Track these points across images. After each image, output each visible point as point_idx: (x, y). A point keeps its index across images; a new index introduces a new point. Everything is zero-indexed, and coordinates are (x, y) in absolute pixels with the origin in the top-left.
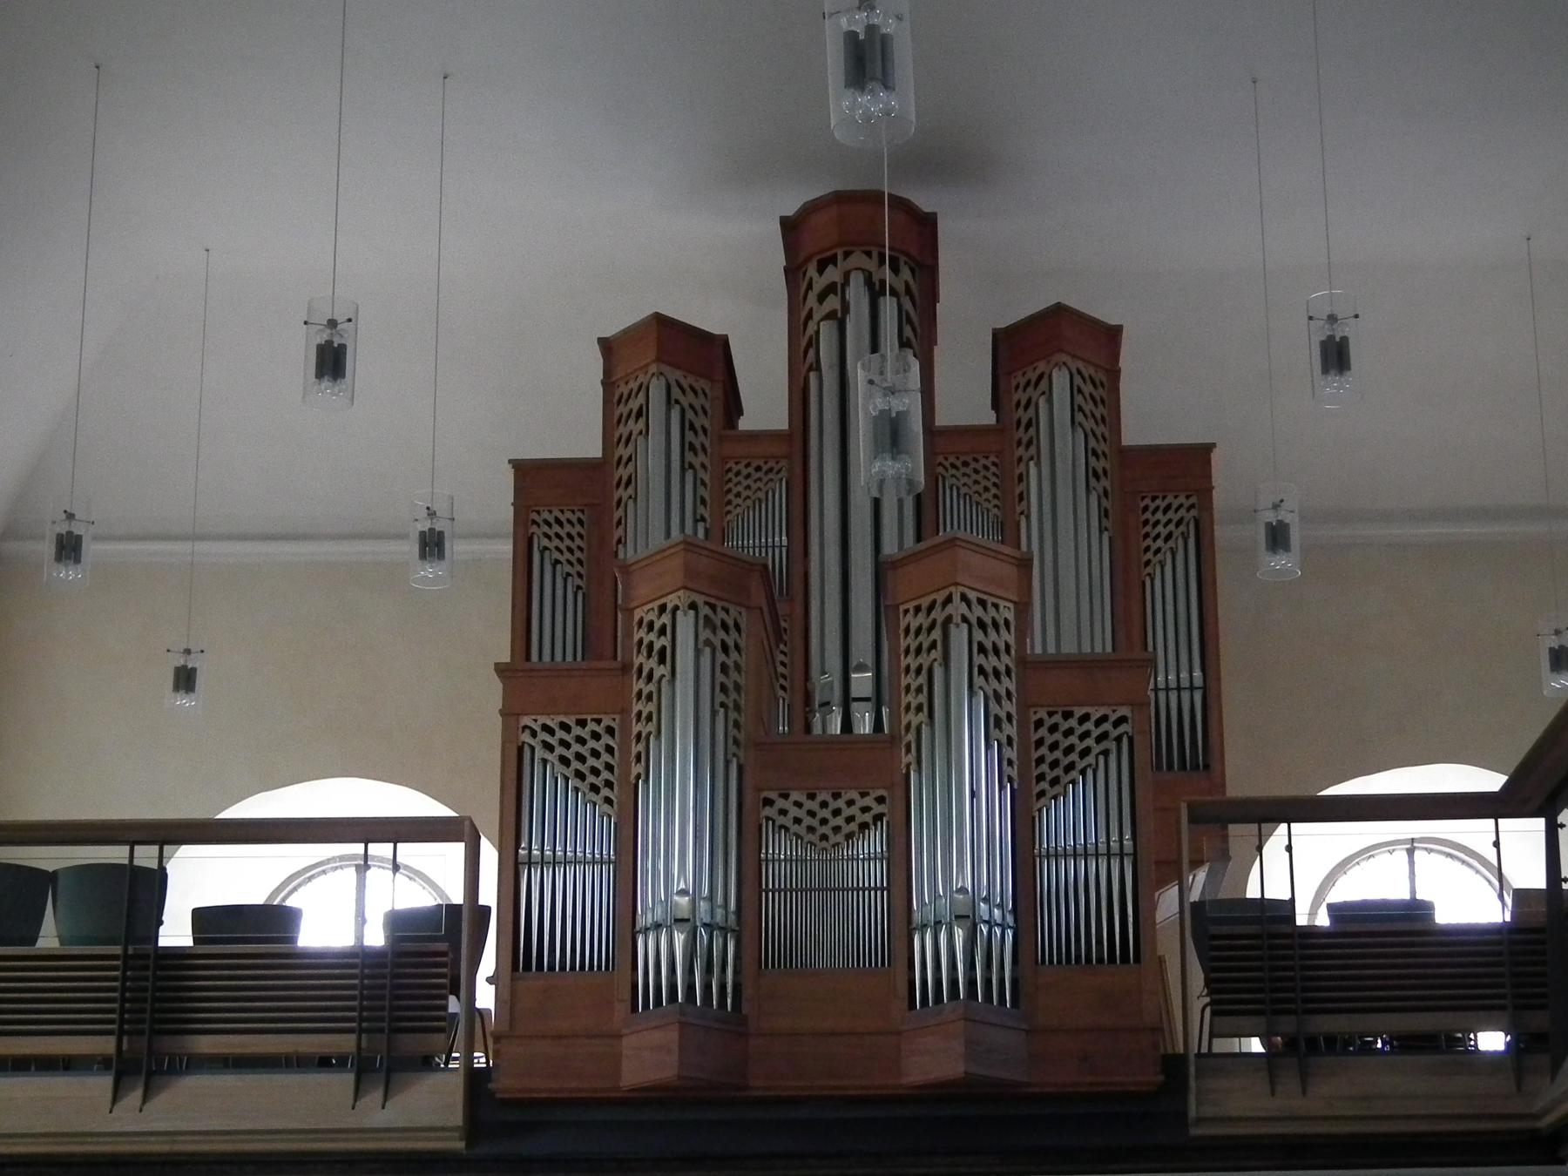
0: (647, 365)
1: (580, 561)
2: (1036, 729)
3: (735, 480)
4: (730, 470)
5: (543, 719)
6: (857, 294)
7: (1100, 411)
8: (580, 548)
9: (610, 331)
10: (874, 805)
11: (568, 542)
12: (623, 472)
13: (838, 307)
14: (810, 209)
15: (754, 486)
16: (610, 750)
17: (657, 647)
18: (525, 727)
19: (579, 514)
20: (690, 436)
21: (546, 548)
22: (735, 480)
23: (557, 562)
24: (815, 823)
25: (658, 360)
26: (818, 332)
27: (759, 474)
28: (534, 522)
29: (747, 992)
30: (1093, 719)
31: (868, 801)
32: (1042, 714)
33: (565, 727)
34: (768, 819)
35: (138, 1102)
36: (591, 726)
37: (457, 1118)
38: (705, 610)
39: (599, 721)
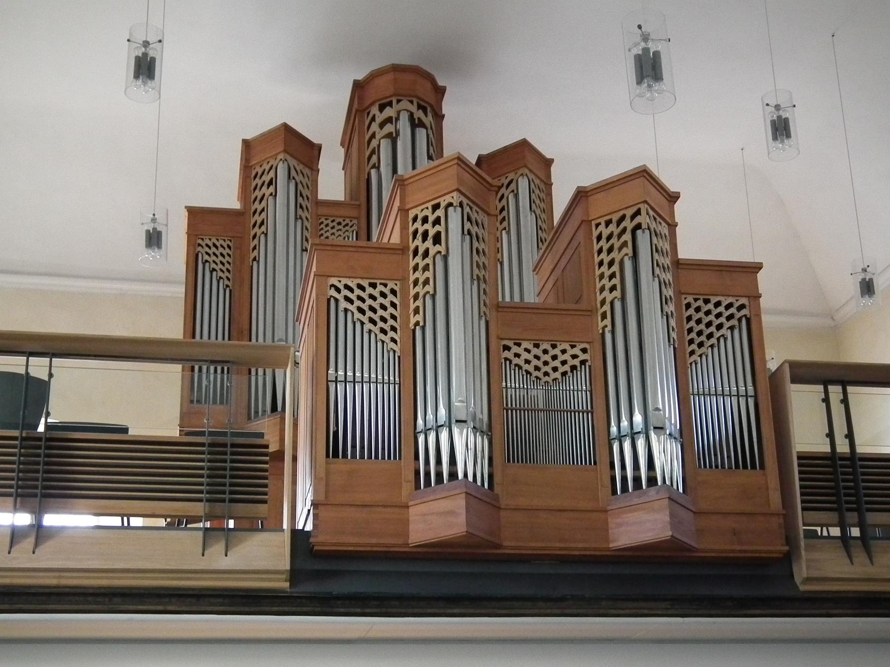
0: (277, 154)
1: (228, 270)
2: (687, 309)
3: (326, 229)
4: (322, 223)
5: (345, 281)
6: (404, 125)
7: (542, 205)
8: (228, 263)
9: (248, 137)
10: (579, 353)
11: (221, 258)
12: (258, 219)
13: (393, 130)
14: (374, 76)
15: (337, 234)
16: (393, 305)
17: (432, 233)
18: (332, 286)
19: (229, 242)
20: (300, 199)
21: (207, 261)
22: (326, 229)
23: (214, 270)
24: (540, 364)
25: (285, 151)
26: (379, 146)
27: (340, 227)
28: (199, 245)
29: (497, 479)
30: (724, 304)
31: (577, 351)
32: (690, 299)
33: (361, 287)
34: (506, 359)
35: (31, 547)
36: (380, 288)
37: (285, 564)
38: (467, 209)
39: (385, 285)
